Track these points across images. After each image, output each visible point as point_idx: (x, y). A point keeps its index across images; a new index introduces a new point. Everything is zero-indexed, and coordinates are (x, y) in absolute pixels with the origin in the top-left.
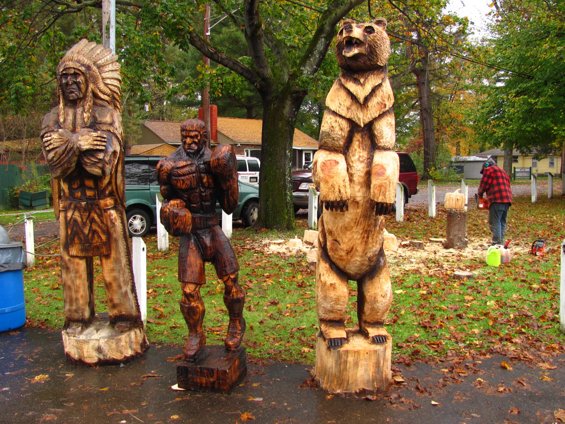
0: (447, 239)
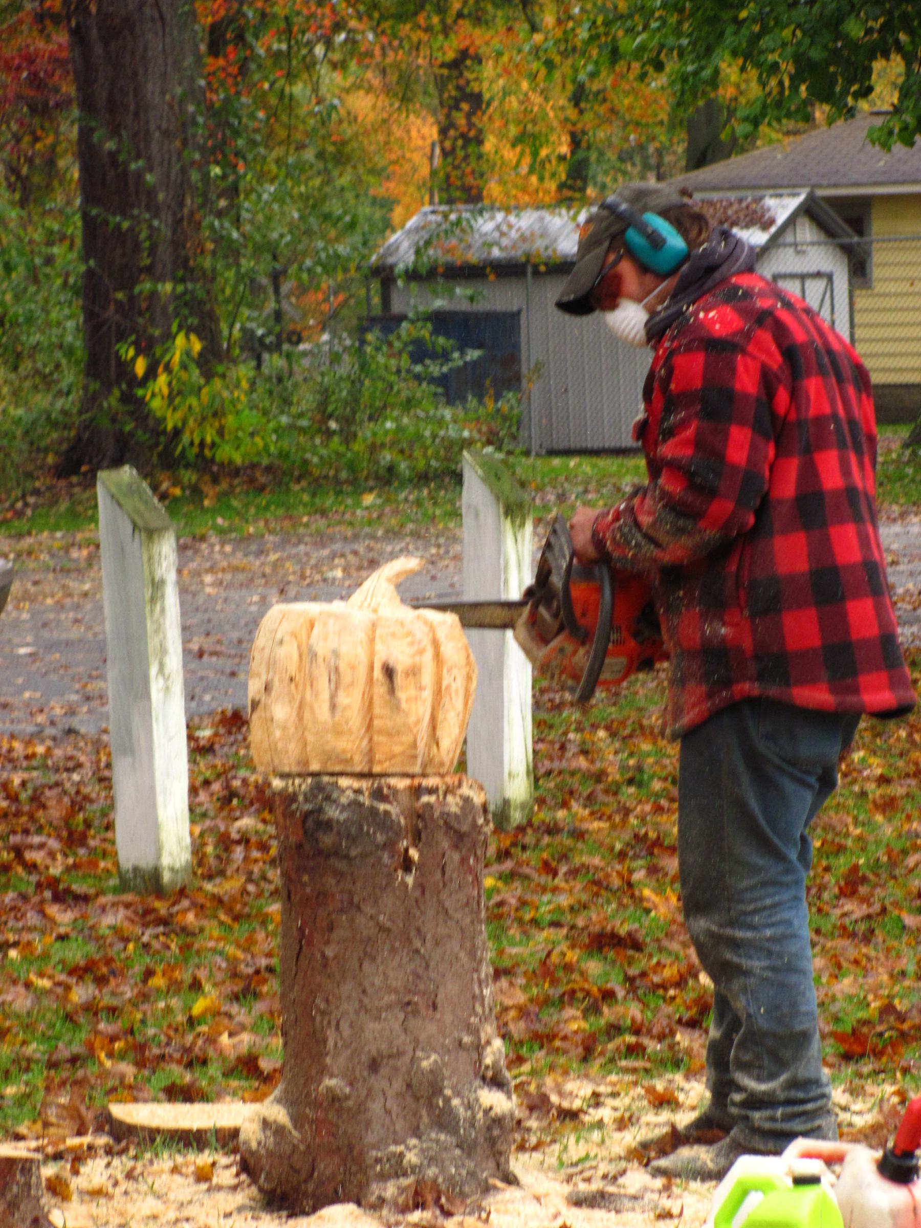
0: (289, 1101)
